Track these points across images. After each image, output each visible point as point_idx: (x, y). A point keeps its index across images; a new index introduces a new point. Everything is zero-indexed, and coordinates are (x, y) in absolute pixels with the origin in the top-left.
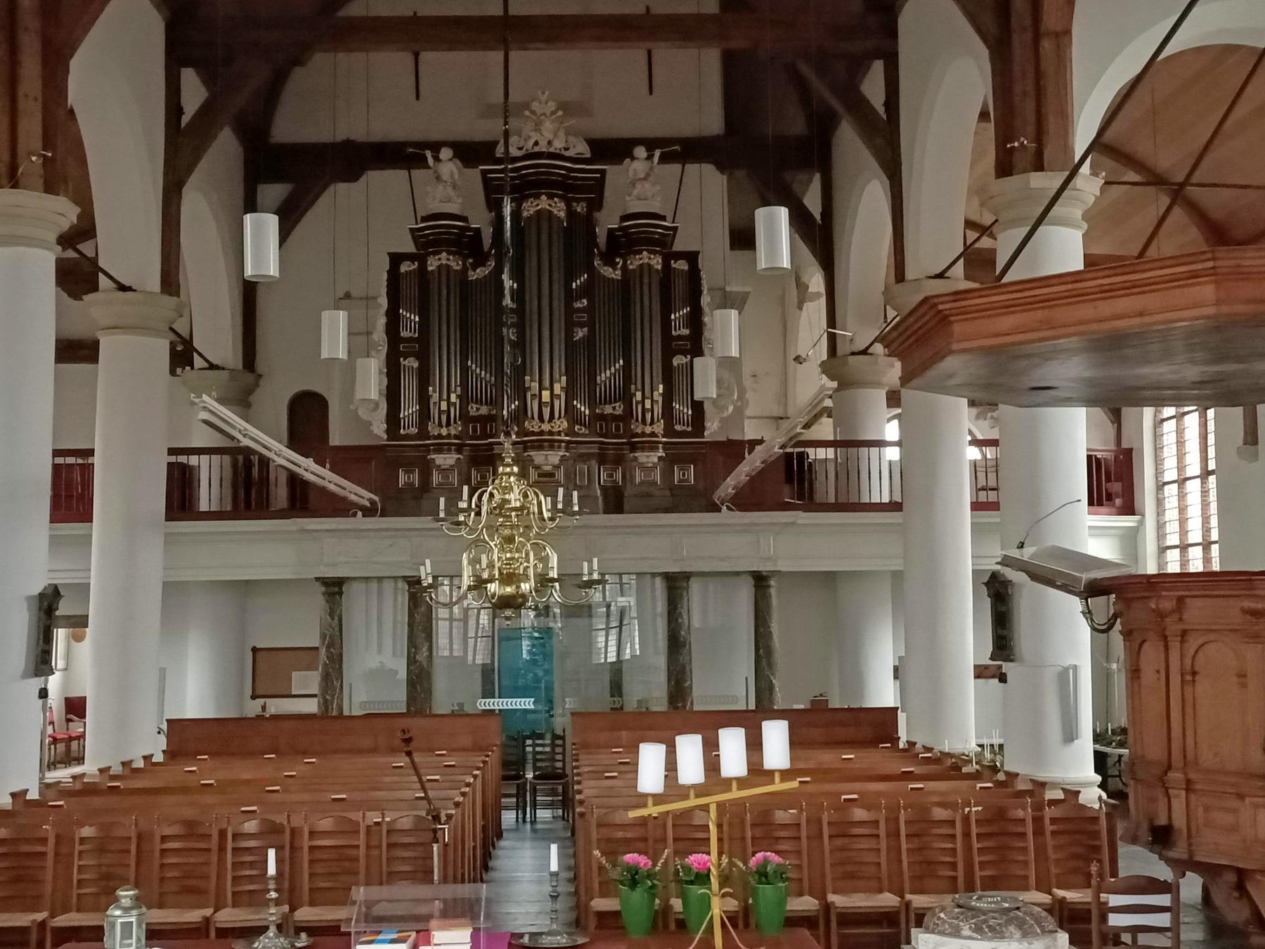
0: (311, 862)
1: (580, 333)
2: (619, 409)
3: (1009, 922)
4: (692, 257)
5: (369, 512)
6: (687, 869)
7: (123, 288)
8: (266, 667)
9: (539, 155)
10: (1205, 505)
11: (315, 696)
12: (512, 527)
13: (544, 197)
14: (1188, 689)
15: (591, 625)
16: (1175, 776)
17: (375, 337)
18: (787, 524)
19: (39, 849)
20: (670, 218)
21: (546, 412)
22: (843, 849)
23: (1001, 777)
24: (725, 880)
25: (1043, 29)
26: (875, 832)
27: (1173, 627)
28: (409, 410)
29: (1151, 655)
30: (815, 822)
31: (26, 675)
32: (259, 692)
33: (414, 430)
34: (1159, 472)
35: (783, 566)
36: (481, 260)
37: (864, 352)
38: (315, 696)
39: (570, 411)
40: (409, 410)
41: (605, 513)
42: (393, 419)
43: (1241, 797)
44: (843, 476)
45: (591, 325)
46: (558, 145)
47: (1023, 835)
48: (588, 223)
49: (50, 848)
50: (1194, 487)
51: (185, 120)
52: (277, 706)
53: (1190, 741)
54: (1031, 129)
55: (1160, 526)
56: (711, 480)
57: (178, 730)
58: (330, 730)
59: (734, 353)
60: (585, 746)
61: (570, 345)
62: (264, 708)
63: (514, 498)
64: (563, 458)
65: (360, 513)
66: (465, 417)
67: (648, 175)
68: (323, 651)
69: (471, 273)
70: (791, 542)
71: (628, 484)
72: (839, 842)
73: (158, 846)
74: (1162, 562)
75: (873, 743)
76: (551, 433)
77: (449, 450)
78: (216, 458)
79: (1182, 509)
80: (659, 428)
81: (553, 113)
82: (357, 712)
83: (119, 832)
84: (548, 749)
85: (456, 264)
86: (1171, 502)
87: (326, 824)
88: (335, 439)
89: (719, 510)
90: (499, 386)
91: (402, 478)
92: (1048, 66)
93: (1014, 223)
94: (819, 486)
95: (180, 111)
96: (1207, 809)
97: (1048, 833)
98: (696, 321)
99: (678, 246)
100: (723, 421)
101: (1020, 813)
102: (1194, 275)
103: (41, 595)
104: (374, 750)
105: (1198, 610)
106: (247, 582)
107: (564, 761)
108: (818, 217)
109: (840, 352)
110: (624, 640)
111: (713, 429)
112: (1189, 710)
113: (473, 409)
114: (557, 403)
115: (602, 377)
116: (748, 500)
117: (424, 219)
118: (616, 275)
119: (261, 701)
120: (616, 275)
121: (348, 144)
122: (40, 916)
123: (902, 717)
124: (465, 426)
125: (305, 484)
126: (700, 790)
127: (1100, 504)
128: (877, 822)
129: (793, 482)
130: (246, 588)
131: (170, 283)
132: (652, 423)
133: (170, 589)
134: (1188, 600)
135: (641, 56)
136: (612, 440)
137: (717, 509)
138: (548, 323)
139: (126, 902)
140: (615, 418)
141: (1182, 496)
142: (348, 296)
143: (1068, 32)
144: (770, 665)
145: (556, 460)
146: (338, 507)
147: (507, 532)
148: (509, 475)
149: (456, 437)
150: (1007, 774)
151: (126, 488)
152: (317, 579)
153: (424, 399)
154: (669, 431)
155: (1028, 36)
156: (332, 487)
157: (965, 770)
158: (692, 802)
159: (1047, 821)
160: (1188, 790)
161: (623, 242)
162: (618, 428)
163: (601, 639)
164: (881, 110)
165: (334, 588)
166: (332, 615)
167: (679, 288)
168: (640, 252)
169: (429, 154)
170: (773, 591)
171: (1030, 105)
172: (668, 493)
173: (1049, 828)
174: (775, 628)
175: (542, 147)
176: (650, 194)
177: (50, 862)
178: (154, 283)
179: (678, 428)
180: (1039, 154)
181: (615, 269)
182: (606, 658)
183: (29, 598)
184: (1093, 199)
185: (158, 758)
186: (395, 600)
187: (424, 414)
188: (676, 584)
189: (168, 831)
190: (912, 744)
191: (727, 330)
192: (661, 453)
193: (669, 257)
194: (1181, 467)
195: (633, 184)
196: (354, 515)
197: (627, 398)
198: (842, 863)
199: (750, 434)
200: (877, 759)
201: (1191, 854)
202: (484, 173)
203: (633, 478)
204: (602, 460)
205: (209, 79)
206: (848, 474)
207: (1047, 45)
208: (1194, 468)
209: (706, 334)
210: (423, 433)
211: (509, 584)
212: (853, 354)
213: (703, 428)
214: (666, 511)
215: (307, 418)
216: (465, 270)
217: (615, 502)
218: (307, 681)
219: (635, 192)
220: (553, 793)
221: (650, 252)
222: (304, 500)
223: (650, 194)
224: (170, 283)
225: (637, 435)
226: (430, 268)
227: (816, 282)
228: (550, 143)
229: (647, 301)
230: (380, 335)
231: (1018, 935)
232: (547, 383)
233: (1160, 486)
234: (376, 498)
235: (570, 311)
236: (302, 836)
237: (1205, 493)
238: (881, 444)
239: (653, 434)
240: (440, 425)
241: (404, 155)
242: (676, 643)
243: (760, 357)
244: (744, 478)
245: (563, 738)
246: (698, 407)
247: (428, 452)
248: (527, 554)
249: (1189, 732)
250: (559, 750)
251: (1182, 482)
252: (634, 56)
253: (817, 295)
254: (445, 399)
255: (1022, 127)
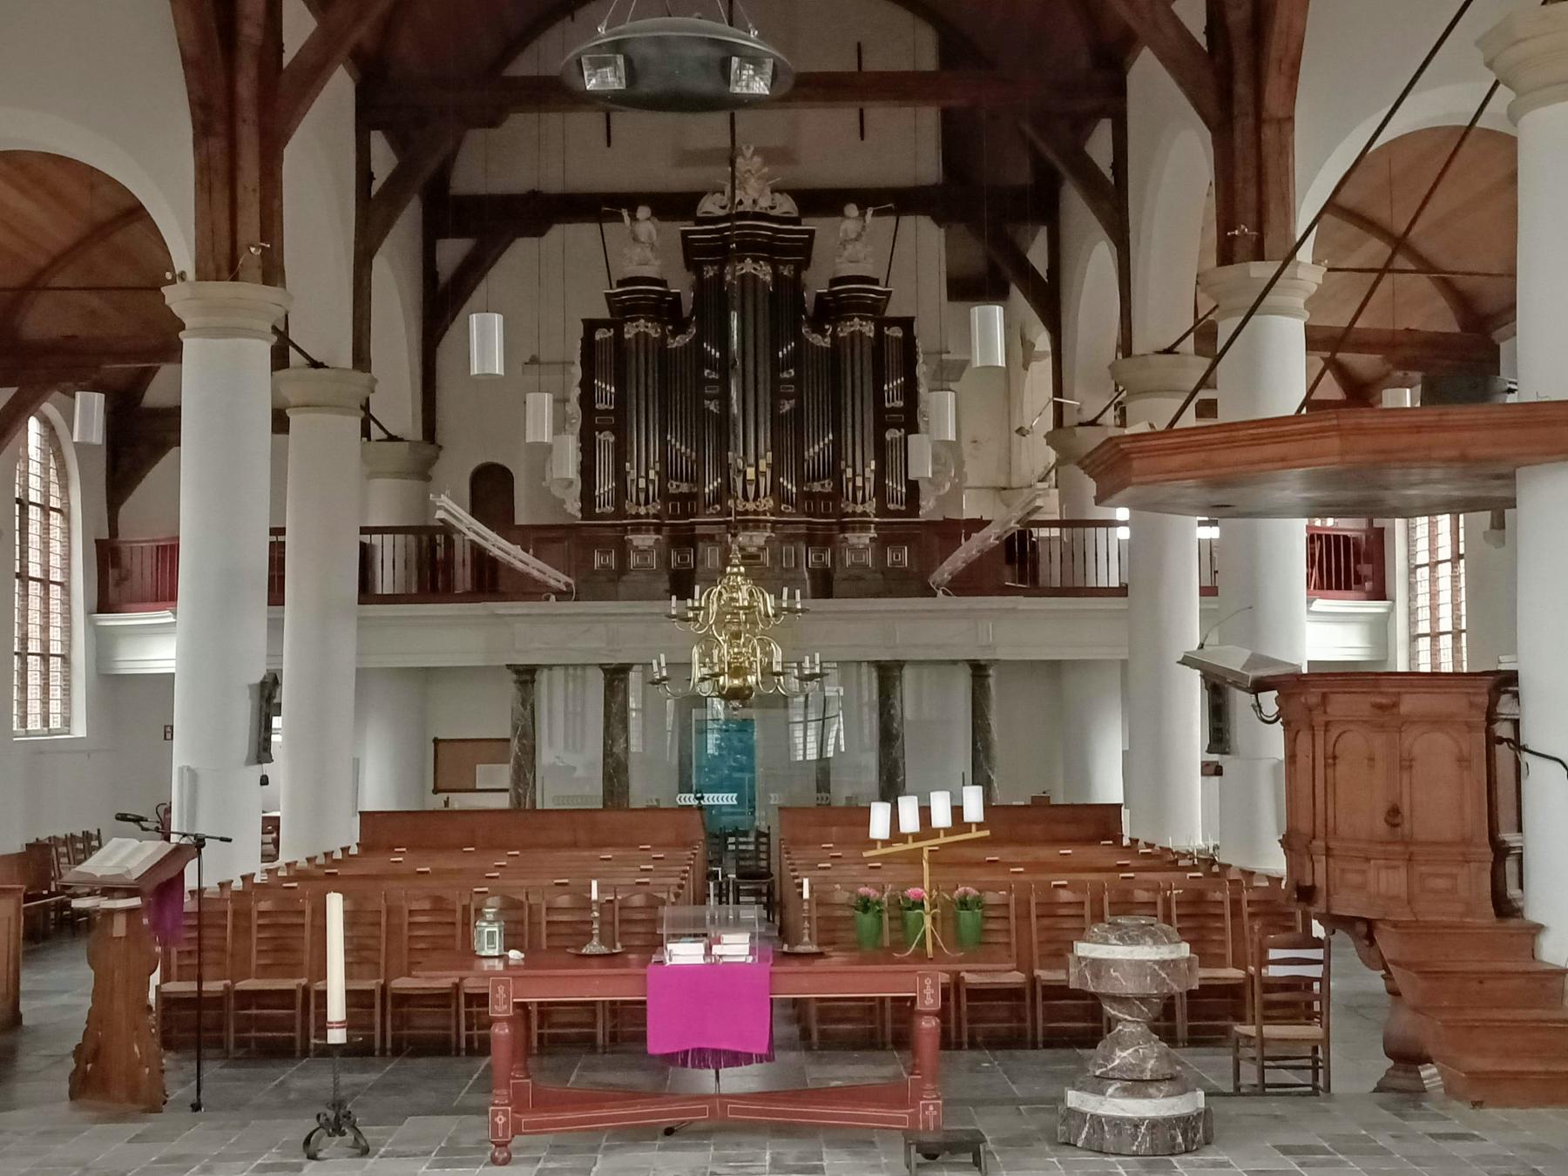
0: (548, 936)
1: (787, 406)
2: (828, 486)
3: (1145, 933)
4: (907, 323)
5: (562, 595)
6: (906, 899)
7: (315, 365)
8: (449, 760)
9: (744, 215)
10: (1455, 590)
11: (506, 790)
12: (739, 623)
13: (749, 260)
14: (1330, 771)
15: (787, 717)
16: (1319, 844)
17: (569, 408)
18: (1007, 610)
19: (298, 920)
20: (882, 282)
21: (751, 490)
22: (1048, 929)
23: (1216, 869)
24: (934, 905)
25: (1265, 115)
26: (1080, 912)
27: (1319, 719)
28: (605, 486)
29: (1304, 739)
30: (1024, 904)
31: (249, 762)
32: (441, 785)
33: (610, 509)
34: (1411, 554)
35: (1003, 654)
36: (681, 328)
37: (1093, 423)
38: (506, 790)
39: (776, 489)
40: (605, 486)
41: (813, 597)
42: (588, 497)
43: (1368, 860)
44: (1068, 557)
45: (798, 397)
46: (764, 203)
47: (1221, 917)
48: (797, 286)
49: (308, 919)
50: (1445, 570)
51: (376, 186)
52: (460, 801)
53: (1330, 812)
54: (1252, 217)
55: (1412, 612)
56: (926, 563)
57: (369, 819)
58: (525, 824)
59: (951, 436)
60: (795, 842)
61: (777, 421)
62: (446, 803)
63: (742, 597)
64: (768, 540)
65: (553, 597)
66: (664, 495)
67: (859, 235)
68: (515, 744)
69: (670, 340)
70: (1012, 628)
71: (838, 567)
72: (1046, 922)
73: (407, 919)
74: (1413, 656)
75: (1092, 840)
76: (756, 513)
77: (647, 531)
78: (400, 538)
79: (1434, 595)
80: (871, 506)
81: (759, 170)
82: (549, 805)
83: (371, 907)
84: (752, 847)
85: (654, 332)
86: (1423, 588)
87: (564, 901)
88: (521, 519)
89: (935, 595)
90: (700, 462)
91: (598, 560)
92: (1269, 148)
93: (1231, 312)
94: (1043, 567)
95: (371, 177)
96: (1343, 870)
97: (1245, 916)
98: (910, 392)
99: (891, 312)
100: (938, 499)
101: (1218, 896)
102: (1322, 430)
103: (263, 684)
104: (575, 845)
105: (1340, 705)
106: (427, 669)
107: (768, 859)
108: (1044, 275)
109: (1066, 422)
110: (823, 734)
111: (929, 508)
112: (1330, 790)
113: (673, 487)
114: (762, 480)
115: (811, 452)
116: (968, 583)
117: (621, 283)
118: (826, 343)
119: (444, 796)
120: (826, 343)
121: (534, 195)
122: (304, 981)
123: (1125, 815)
124: (664, 503)
125: (494, 561)
126: (917, 837)
127: (1348, 588)
128: (1082, 903)
129: (1017, 564)
130: (427, 676)
131: (361, 359)
132: (864, 501)
133: (361, 674)
134: (1331, 696)
135: (855, 114)
136: (818, 519)
137: (929, 592)
138: (754, 391)
139: (490, 917)
140: (822, 496)
141: (1433, 580)
142: (534, 360)
143: (1291, 119)
144: (988, 757)
145: (761, 542)
146: (530, 590)
147: (734, 628)
148: (737, 574)
149: (655, 516)
150: (1221, 865)
151: (320, 574)
152: (509, 666)
153: (620, 475)
154: (882, 510)
155: (1250, 121)
156: (536, 573)
157: (1181, 863)
158: (911, 845)
159: (1245, 904)
160: (1327, 856)
161: (833, 308)
162: (827, 507)
163: (799, 733)
164: (1108, 173)
165: (526, 675)
166: (523, 704)
167: (893, 356)
168: (851, 319)
169: (625, 213)
170: (992, 681)
171: (1251, 195)
172: (879, 576)
173: (1246, 910)
174: (994, 720)
175: (747, 207)
176: (861, 256)
177: (307, 934)
178: (347, 360)
179: (891, 506)
180: (1260, 242)
181: (824, 336)
182: (805, 755)
183: (251, 686)
184: (1315, 288)
185: (354, 851)
186: (566, 688)
187: (621, 492)
188: (888, 674)
189: (415, 906)
190: (1134, 841)
191: (942, 412)
192: (872, 534)
193: (882, 323)
194: (1433, 550)
195: (844, 243)
196: (547, 599)
197: (835, 473)
198: (1049, 942)
199: (969, 511)
200: (1100, 853)
201: (1328, 908)
202: (685, 234)
203: (843, 560)
204: (810, 540)
205: (399, 143)
206: (1075, 555)
207: (1268, 133)
208: (1445, 553)
209: (921, 406)
210: (620, 512)
211: (737, 677)
212: (1081, 424)
213: (918, 507)
214: (878, 595)
215: (491, 490)
216: (663, 338)
217: (824, 585)
218: (503, 774)
219: (846, 253)
220: (757, 893)
221: (861, 318)
222: (490, 580)
223: (861, 256)
224: (361, 359)
225: (847, 515)
226: (627, 336)
227: (1043, 341)
228: (755, 202)
229: (859, 372)
230: (574, 408)
231: (1150, 942)
232: (752, 460)
233: (1413, 569)
234: (571, 581)
235: (776, 381)
236: (540, 911)
237: (1455, 578)
238: (1111, 524)
239: (865, 514)
240: (638, 504)
241: (597, 207)
242: (888, 737)
243: (987, 412)
244: (960, 565)
245: (767, 835)
246: (913, 488)
247: (626, 532)
248: (754, 649)
249: (1330, 806)
250: (763, 848)
251: (1434, 565)
252: (846, 116)
253: (1042, 355)
254: (643, 475)
255: (1246, 218)
